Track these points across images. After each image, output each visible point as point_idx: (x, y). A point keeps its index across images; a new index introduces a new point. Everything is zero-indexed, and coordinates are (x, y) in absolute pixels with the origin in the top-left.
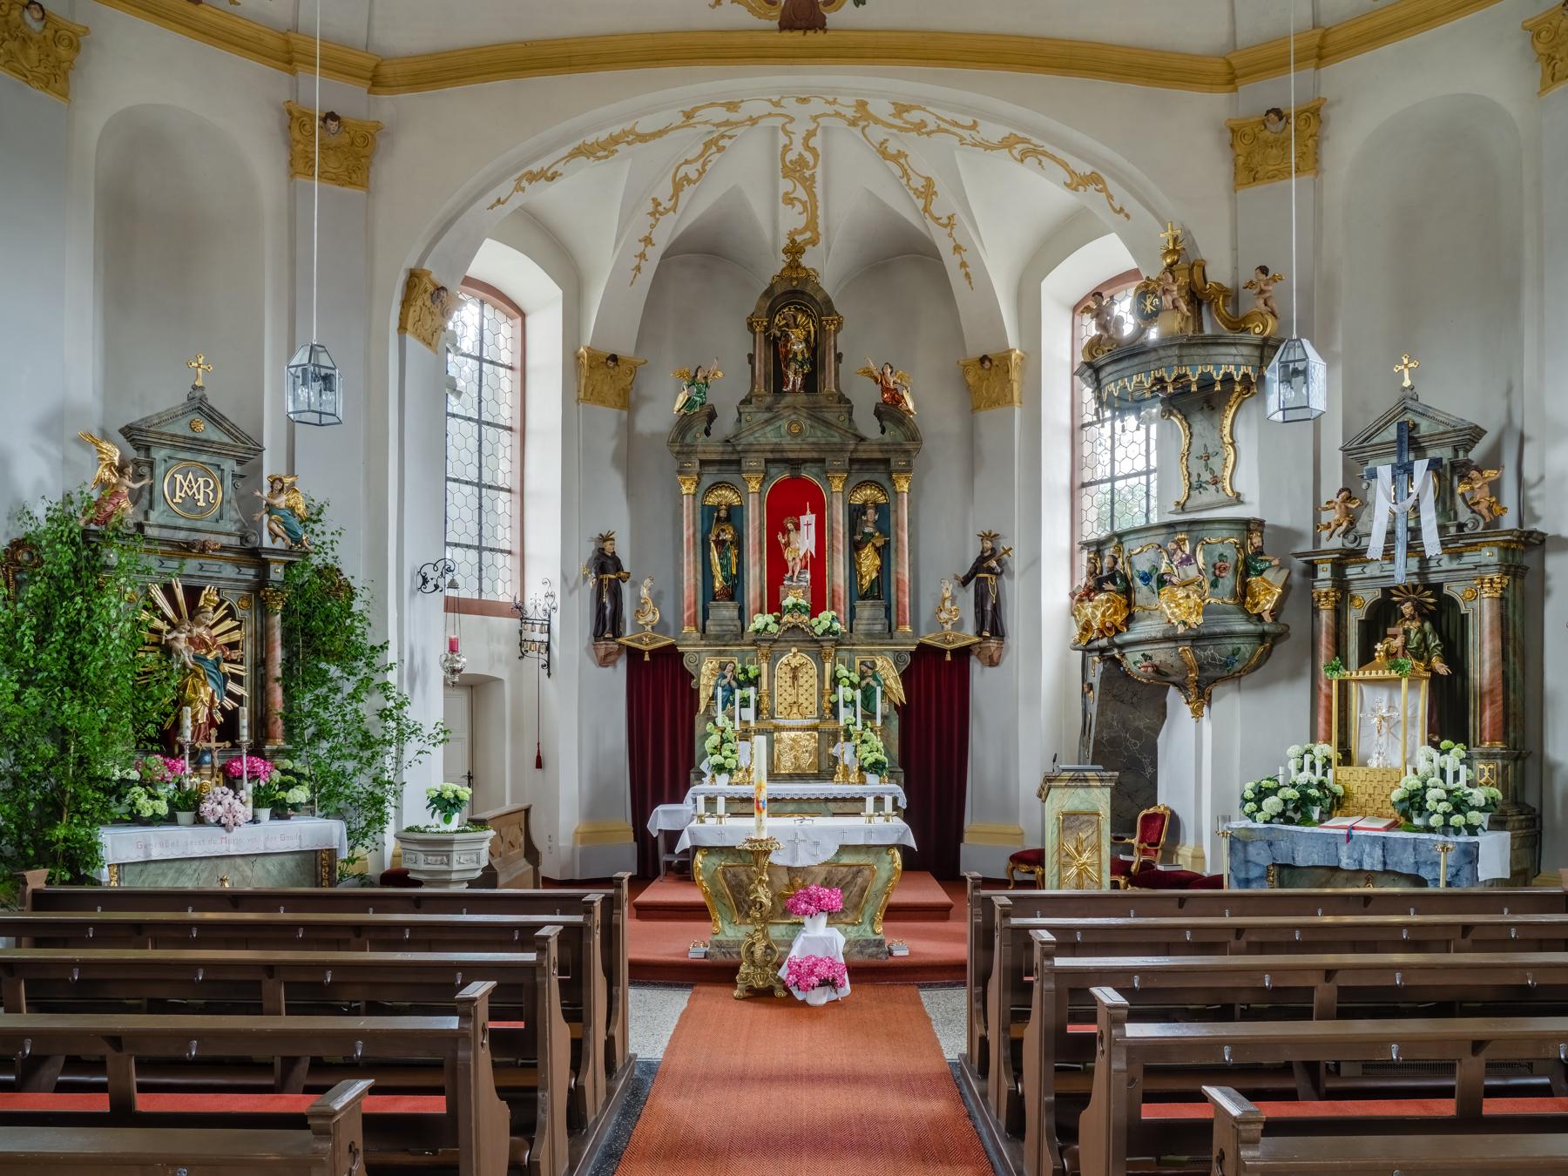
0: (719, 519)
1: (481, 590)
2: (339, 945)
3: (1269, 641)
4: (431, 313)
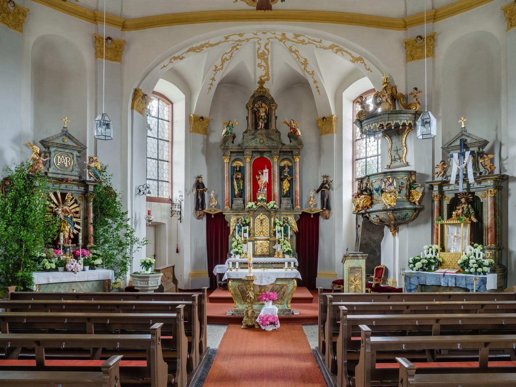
0: (236, 171)
1: (158, 194)
2: (111, 311)
3: (417, 211)
4: (142, 103)
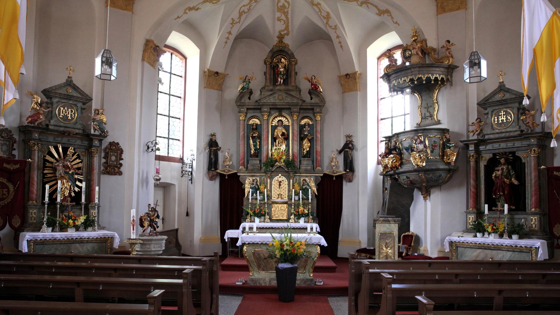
0: (253, 129)
1: (168, 153)
4: (154, 55)
